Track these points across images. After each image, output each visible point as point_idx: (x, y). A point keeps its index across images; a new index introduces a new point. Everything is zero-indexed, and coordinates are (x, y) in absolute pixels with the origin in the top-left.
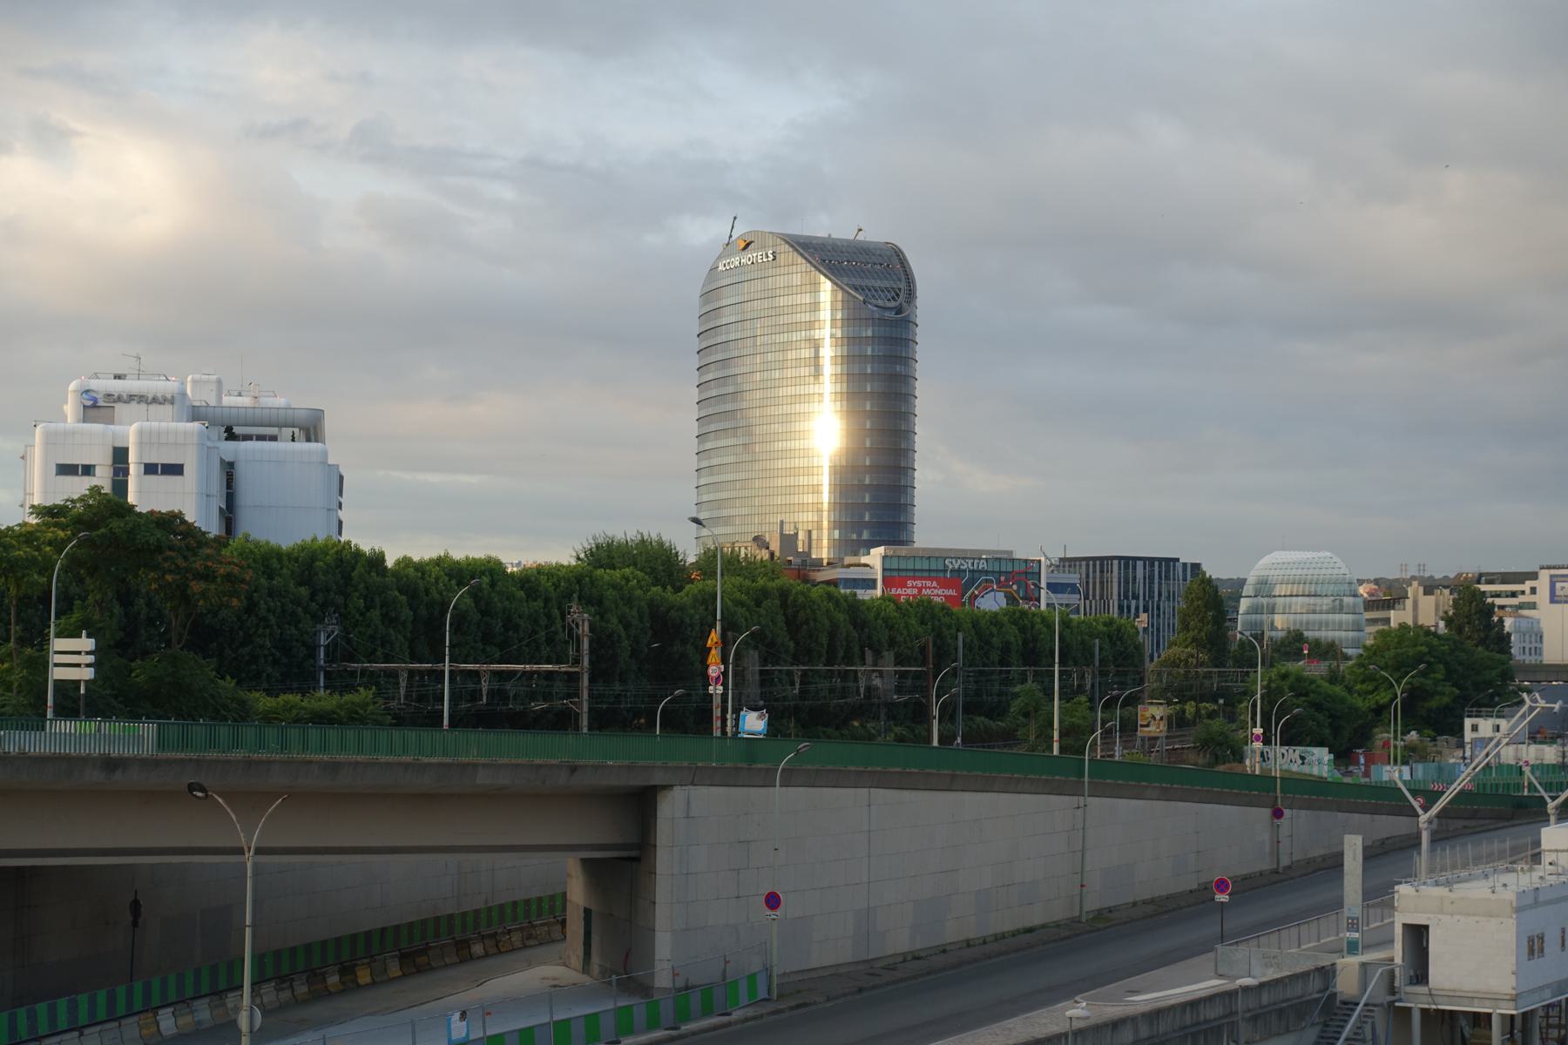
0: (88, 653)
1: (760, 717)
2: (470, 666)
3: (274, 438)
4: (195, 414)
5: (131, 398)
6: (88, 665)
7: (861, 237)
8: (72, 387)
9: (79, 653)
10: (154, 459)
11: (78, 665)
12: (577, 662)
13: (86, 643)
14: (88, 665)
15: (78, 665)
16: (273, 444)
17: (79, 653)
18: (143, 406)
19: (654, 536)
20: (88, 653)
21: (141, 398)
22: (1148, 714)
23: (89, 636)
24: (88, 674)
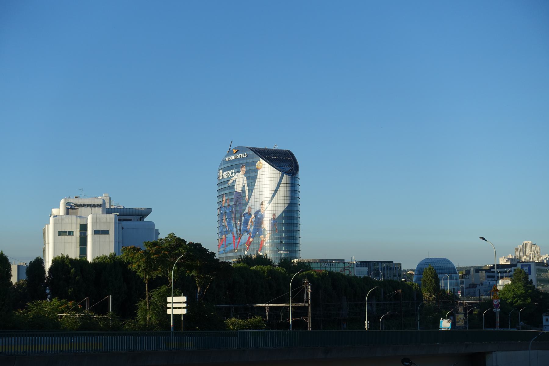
0: (184, 303)
1: (448, 322)
2: (261, 305)
3: (130, 220)
4: (109, 211)
5: (84, 205)
6: (184, 308)
7: (276, 148)
8: (62, 201)
9: (180, 303)
10: (98, 228)
11: (180, 308)
12: (307, 302)
13: (183, 299)
14: (184, 308)
15: (180, 308)
16: (128, 223)
17: (180, 303)
18: (89, 208)
19: (60, 255)
20: (184, 303)
21: (89, 205)
22: (459, 318)
23: (184, 296)
24: (184, 311)
